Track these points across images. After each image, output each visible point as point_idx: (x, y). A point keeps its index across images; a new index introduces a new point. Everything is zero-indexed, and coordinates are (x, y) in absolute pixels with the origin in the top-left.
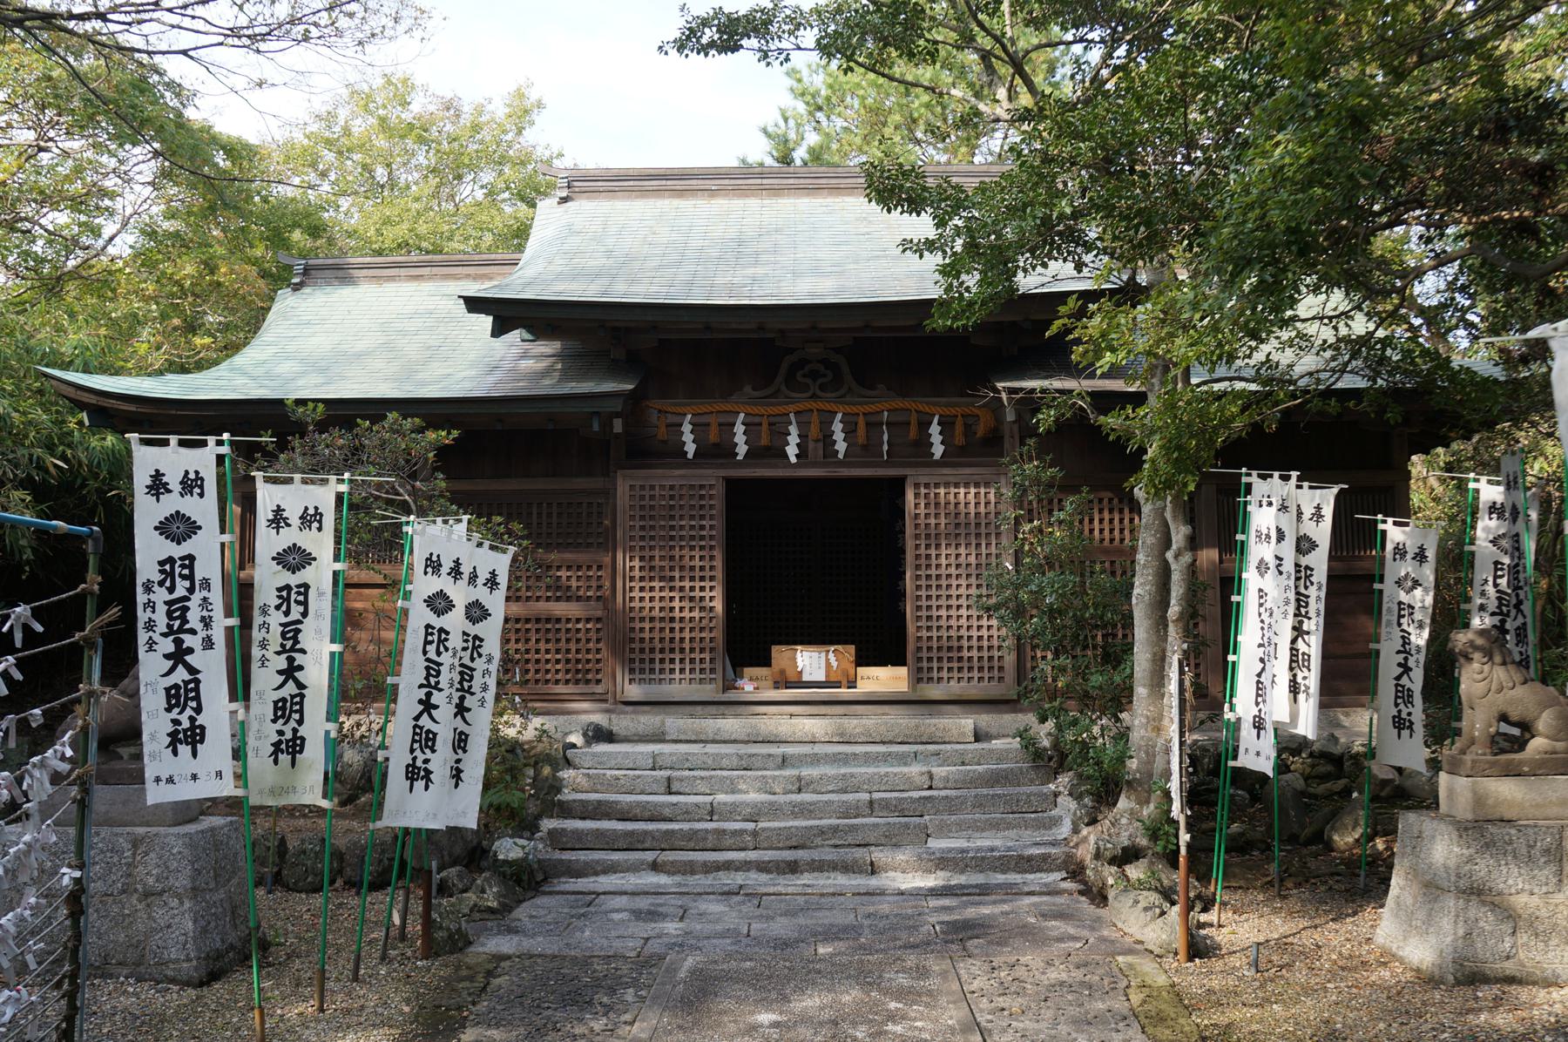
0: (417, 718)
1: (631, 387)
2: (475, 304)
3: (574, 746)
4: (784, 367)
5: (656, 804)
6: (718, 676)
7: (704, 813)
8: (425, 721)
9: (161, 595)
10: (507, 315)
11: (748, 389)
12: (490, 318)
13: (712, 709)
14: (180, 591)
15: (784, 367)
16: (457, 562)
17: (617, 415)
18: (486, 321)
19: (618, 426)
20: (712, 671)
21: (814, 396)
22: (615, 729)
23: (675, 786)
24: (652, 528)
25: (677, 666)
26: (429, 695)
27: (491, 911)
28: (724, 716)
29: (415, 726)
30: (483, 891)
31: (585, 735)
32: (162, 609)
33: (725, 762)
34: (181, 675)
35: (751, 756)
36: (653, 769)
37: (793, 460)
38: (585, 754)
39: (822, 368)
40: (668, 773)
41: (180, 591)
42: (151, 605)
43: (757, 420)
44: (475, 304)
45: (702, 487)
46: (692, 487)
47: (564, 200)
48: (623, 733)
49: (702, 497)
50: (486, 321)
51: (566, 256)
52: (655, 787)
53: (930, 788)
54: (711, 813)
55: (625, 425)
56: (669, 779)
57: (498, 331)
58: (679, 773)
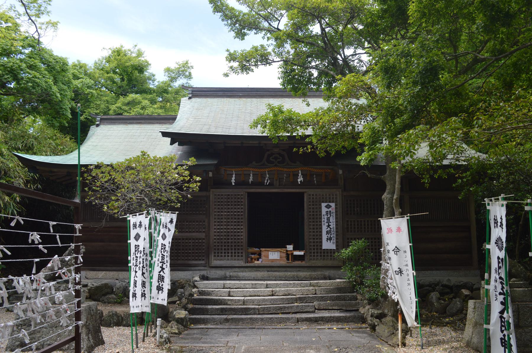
0: (160, 272)
1: (216, 162)
2: (165, 134)
3: (197, 281)
4: (266, 155)
5: (225, 300)
6: (244, 258)
7: (241, 303)
8: (162, 273)
9: (326, 217)
10: (176, 138)
11: (254, 163)
12: (170, 139)
13: (242, 269)
14: (329, 216)
15: (266, 155)
16: (140, 222)
17: (211, 171)
18: (169, 140)
19: (211, 174)
20: (242, 256)
21: (276, 166)
22: (209, 276)
23: (232, 294)
24: (222, 208)
25: (230, 255)
26: (162, 265)
27: (175, 333)
28: (245, 271)
29: (159, 275)
30: (172, 327)
31: (200, 277)
32: (326, 219)
33: (247, 286)
34: (329, 229)
35: (256, 284)
36: (224, 288)
37: (233, 184)
38: (201, 284)
39: (278, 156)
40: (229, 290)
41: (329, 216)
42: (324, 218)
43: (257, 173)
44: (165, 134)
45: (238, 195)
46: (235, 195)
47: (190, 98)
48: (212, 277)
49: (238, 198)
50: (169, 140)
51: (192, 117)
52: (224, 294)
53: (315, 294)
54: (244, 302)
55: (213, 174)
56: (229, 292)
57: (172, 143)
58: (232, 290)
